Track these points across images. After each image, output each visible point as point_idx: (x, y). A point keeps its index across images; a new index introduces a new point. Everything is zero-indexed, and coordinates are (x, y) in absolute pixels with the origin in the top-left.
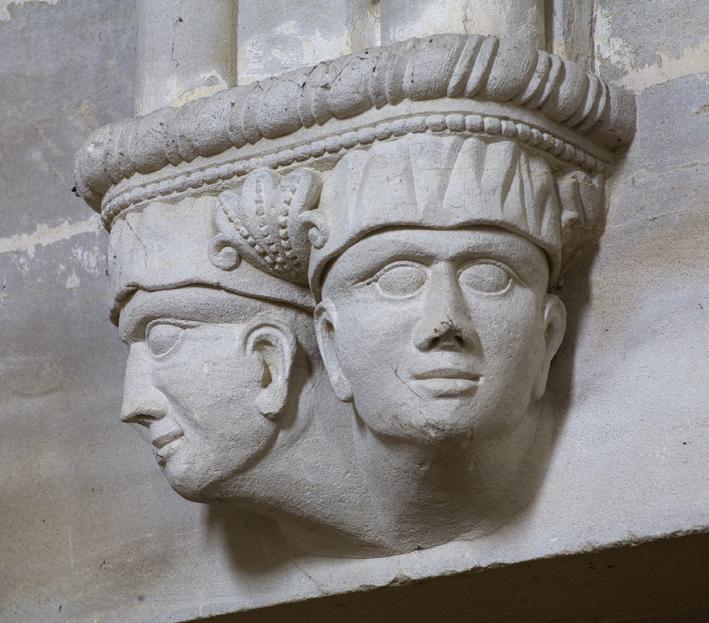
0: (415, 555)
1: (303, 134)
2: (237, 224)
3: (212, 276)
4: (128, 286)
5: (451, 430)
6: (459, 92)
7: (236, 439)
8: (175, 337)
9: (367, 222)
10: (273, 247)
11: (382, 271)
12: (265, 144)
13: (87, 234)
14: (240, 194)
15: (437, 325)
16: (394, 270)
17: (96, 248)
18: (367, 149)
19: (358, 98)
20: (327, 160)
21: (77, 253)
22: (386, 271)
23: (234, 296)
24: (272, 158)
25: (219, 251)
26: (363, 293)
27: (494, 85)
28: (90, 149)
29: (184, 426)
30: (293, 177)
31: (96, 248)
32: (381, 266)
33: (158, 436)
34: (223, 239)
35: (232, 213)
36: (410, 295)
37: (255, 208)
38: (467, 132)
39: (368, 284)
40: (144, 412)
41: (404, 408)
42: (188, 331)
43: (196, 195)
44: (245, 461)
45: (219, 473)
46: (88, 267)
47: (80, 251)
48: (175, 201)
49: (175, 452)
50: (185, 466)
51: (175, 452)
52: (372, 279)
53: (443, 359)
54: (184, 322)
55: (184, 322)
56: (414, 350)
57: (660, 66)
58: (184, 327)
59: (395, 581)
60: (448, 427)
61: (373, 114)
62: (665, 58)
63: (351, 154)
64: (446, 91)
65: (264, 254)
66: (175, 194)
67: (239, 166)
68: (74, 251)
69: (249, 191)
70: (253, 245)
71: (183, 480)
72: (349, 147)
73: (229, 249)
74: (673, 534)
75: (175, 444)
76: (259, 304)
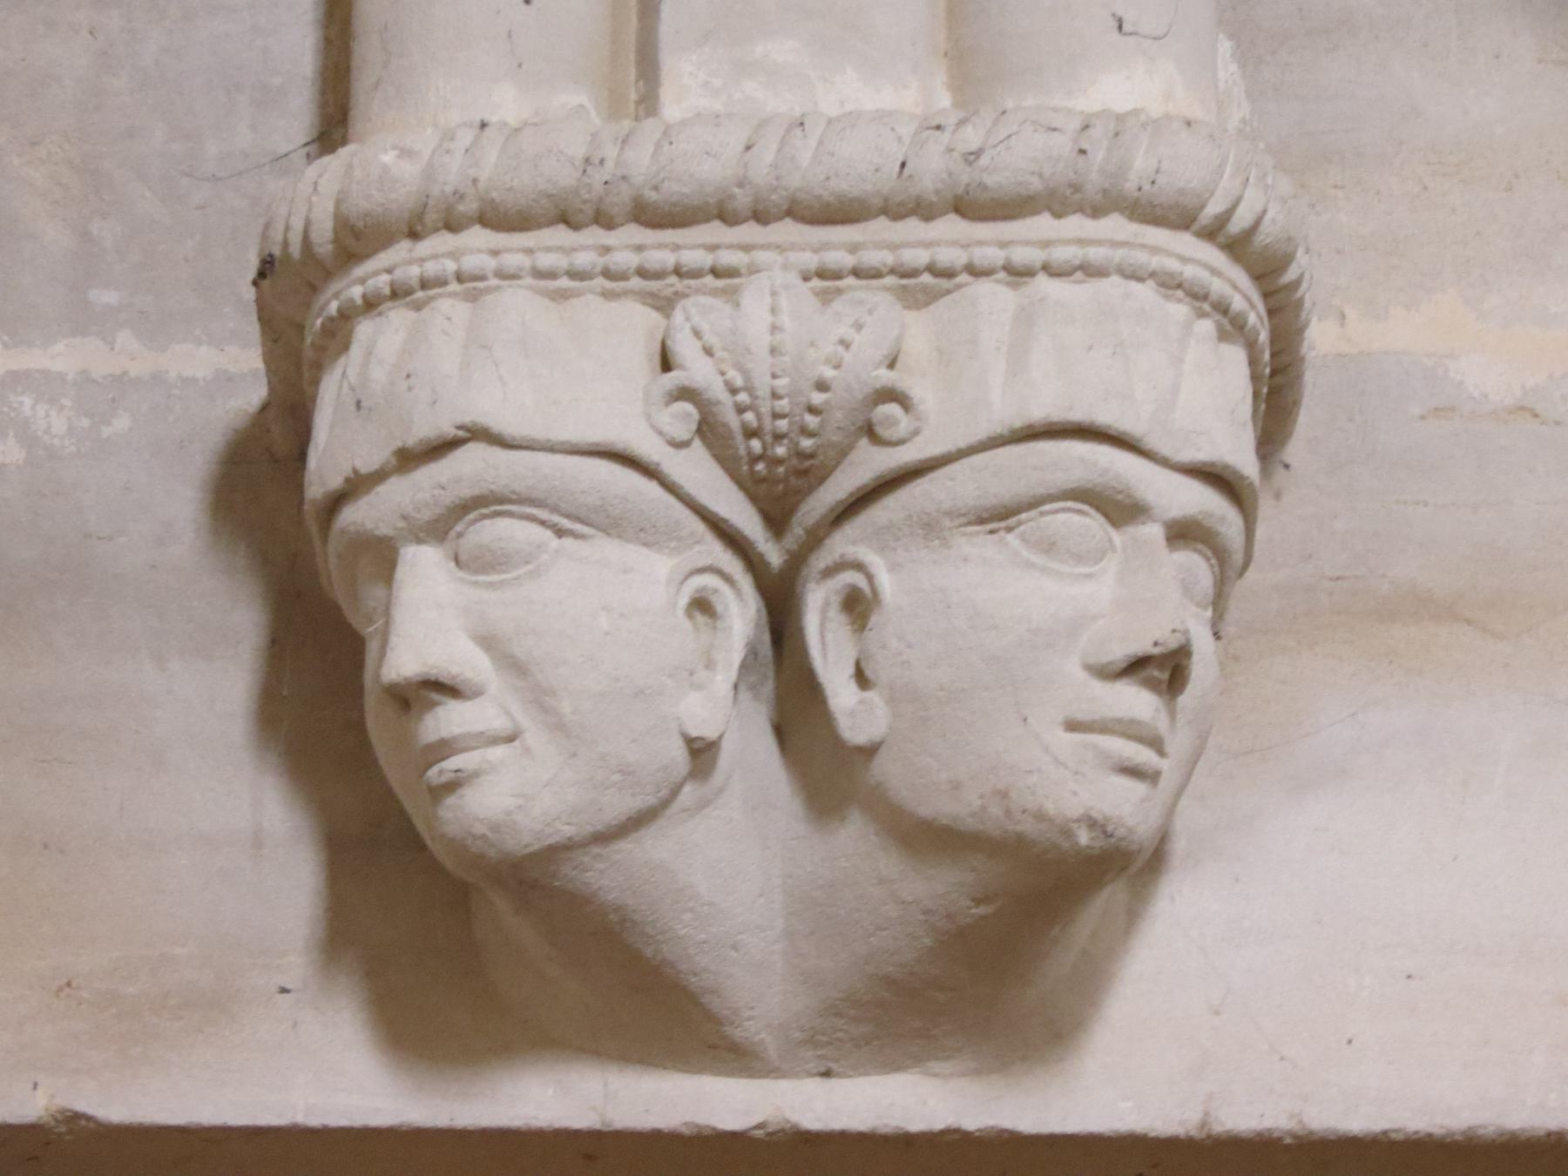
0: (814, 1085)
1: (881, 228)
2: (722, 360)
3: (650, 448)
4: (460, 427)
5: (1122, 839)
6: (1211, 234)
7: (626, 771)
8: (540, 546)
9: (1041, 410)
10: (783, 424)
11: (1033, 513)
12: (787, 231)
13: (45, 373)
14: (737, 305)
15: (1158, 635)
16: (1061, 517)
17: (66, 402)
18: (1014, 286)
19: (1036, 185)
20: (925, 289)
21: (21, 403)
22: (1042, 514)
23: (672, 500)
24: (811, 260)
25: (668, 404)
26: (978, 546)
27: (1268, 235)
28: (388, 158)
29: (524, 721)
30: (861, 302)
31: (66, 402)
32: (1034, 503)
33: (457, 731)
34: (687, 383)
35: (711, 339)
36: (1087, 570)
37: (767, 339)
38: (1206, 307)
39: (992, 532)
40: (444, 679)
41: (1034, 779)
42: (568, 542)
43: (607, 295)
44: (623, 818)
45: (568, 831)
46: (47, 432)
47: (27, 401)
48: (561, 296)
49: (476, 774)
50: (510, 802)
51: (476, 774)
52: (1003, 524)
53: (1136, 701)
54: (566, 523)
55: (566, 523)
56: (1081, 675)
57: (1342, 325)
58: (560, 533)
59: (760, 1126)
60: (1121, 832)
61: (1042, 225)
62: (1351, 313)
63: (984, 287)
64: (1194, 219)
65: (750, 433)
66: (564, 282)
67: (728, 258)
68: (12, 397)
69: (755, 302)
70: (741, 410)
71: (496, 828)
72: (976, 272)
73: (688, 407)
74: (1385, 1133)
75: (497, 753)
76: (700, 527)
